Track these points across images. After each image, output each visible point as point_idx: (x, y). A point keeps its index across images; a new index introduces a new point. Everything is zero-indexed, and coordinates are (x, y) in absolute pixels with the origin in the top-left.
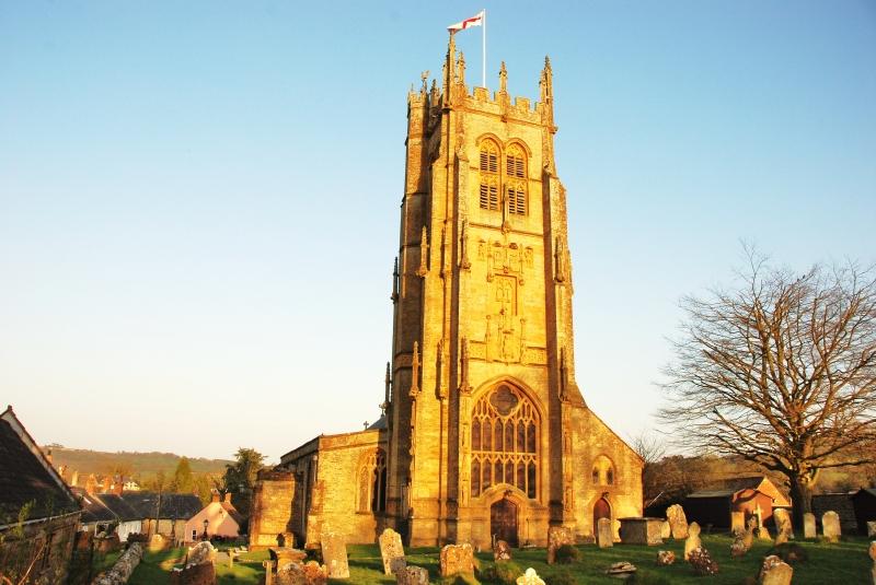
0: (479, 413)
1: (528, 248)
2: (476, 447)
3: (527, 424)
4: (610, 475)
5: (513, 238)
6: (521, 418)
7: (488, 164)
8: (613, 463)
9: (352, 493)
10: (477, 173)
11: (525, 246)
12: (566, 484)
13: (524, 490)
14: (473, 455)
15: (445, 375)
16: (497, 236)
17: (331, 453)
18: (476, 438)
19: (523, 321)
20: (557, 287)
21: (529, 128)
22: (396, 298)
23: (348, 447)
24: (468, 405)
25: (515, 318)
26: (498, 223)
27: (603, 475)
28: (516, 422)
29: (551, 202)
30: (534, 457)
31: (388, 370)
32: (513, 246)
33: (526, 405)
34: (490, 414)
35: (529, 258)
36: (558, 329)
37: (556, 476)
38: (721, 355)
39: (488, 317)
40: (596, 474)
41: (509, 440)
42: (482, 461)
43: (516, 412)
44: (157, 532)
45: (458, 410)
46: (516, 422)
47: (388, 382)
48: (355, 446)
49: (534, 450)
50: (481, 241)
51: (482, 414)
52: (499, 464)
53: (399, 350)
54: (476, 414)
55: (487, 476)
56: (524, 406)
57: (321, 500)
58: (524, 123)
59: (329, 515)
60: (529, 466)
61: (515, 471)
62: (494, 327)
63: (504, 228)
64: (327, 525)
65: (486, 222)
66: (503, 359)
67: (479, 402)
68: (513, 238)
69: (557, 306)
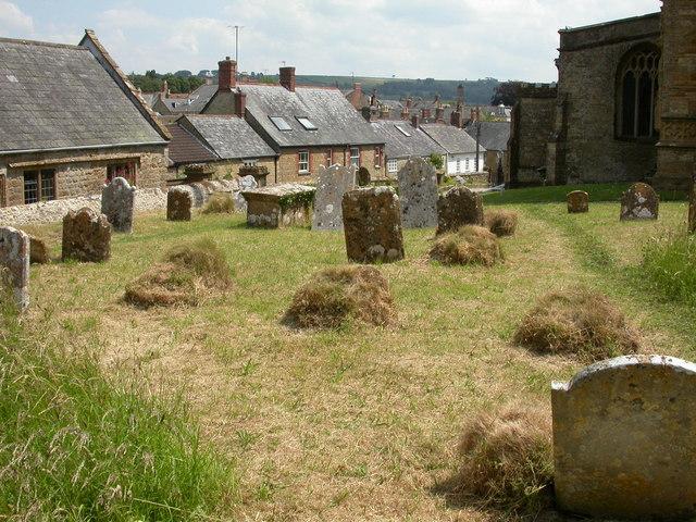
3: (637, 77)
17: (577, 54)
23: (602, 44)
24: (648, 39)
48: (611, 42)
57: (564, 120)
64: (574, 155)
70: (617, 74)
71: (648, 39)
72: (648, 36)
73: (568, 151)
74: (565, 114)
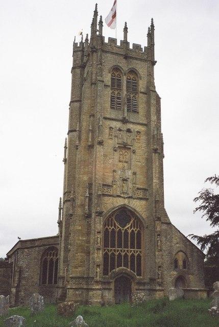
0: (108, 226)
1: (138, 132)
2: (127, 91)
4: (184, 262)
6: (133, 229)
8: (187, 256)
9: (38, 274)
10: (109, 89)
11: (137, 130)
12: (174, 281)
13: (134, 271)
14: (105, 250)
16: (118, 125)
18: (128, 87)
19: (134, 174)
22: (65, 160)
24: (54, 245)
27: (180, 263)
28: (130, 231)
31: (61, 202)
32: (129, 131)
34: (115, 226)
35: (138, 137)
38: (207, 196)
40: (176, 261)
41: (126, 241)
42: (136, 255)
43: (130, 225)
46: (130, 231)
47: (60, 209)
49: (139, 247)
50: (111, 128)
51: (110, 227)
53: (66, 191)
56: (134, 221)
58: (136, 59)
59: (24, 288)
60: (131, 256)
61: (129, 260)
63: (124, 121)
64: (22, 293)
65: (113, 116)
66: (122, 195)
68: (130, 126)
70: (41, 259)
71: (54, 245)
72: (55, 244)
73: (20, 291)
74: (20, 275)
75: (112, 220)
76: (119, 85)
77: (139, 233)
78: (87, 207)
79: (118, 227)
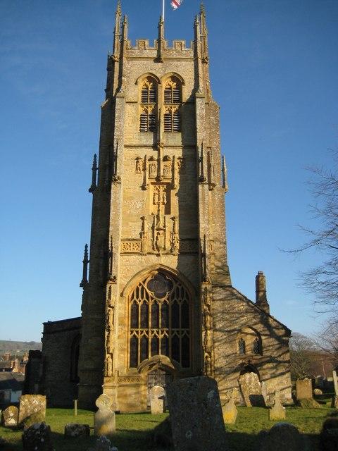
3: (180, 304)
5: (164, 152)
7: (150, 96)
14: (132, 332)
15: (161, 98)
20: (200, 187)
21: (184, 63)
25: (168, 217)
26: (151, 142)
29: (198, 117)
30: (188, 332)
33: (180, 287)
36: (201, 221)
37: (281, 332)
39: (143, 218)
42: (180, 337)
44: (108, 353)
45: (77, 359)
52: (155, 339)
54: (175, 299)
55: (144, 355)
56: (178, 288)
58: (179, 60)
62: (148, 226)
67: (138, 289)
69: (200, 201)
75: (143, 288)
76: (155, 99)
77: (185, 306)
78: (101, 273)
79: (152, 299)
